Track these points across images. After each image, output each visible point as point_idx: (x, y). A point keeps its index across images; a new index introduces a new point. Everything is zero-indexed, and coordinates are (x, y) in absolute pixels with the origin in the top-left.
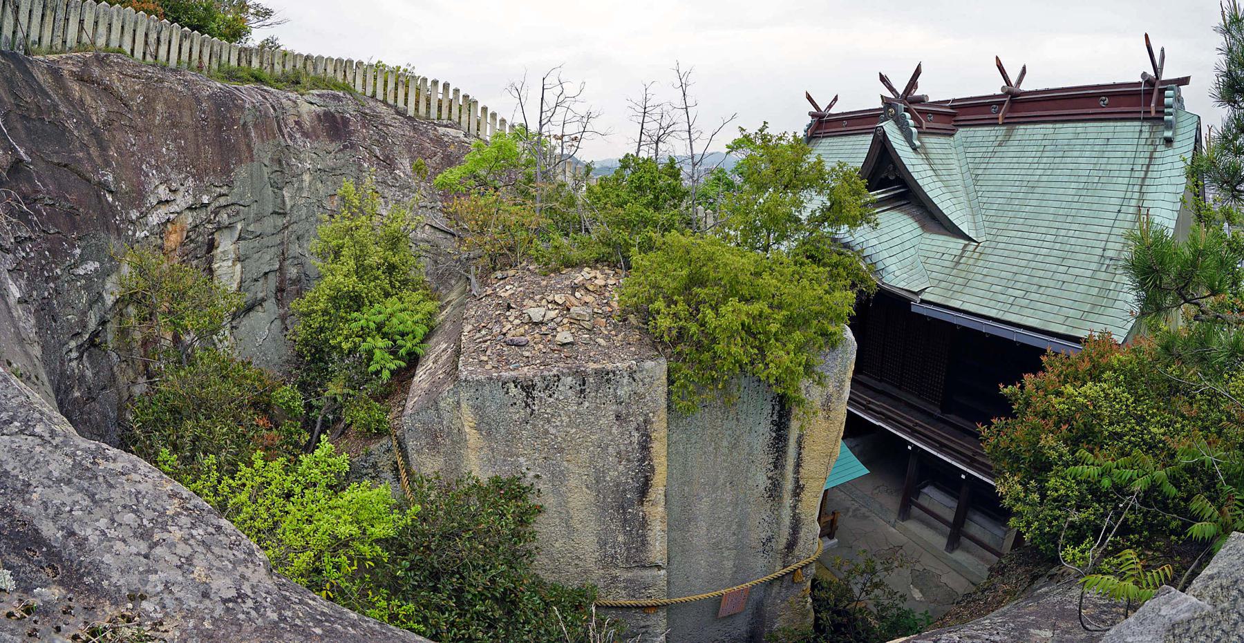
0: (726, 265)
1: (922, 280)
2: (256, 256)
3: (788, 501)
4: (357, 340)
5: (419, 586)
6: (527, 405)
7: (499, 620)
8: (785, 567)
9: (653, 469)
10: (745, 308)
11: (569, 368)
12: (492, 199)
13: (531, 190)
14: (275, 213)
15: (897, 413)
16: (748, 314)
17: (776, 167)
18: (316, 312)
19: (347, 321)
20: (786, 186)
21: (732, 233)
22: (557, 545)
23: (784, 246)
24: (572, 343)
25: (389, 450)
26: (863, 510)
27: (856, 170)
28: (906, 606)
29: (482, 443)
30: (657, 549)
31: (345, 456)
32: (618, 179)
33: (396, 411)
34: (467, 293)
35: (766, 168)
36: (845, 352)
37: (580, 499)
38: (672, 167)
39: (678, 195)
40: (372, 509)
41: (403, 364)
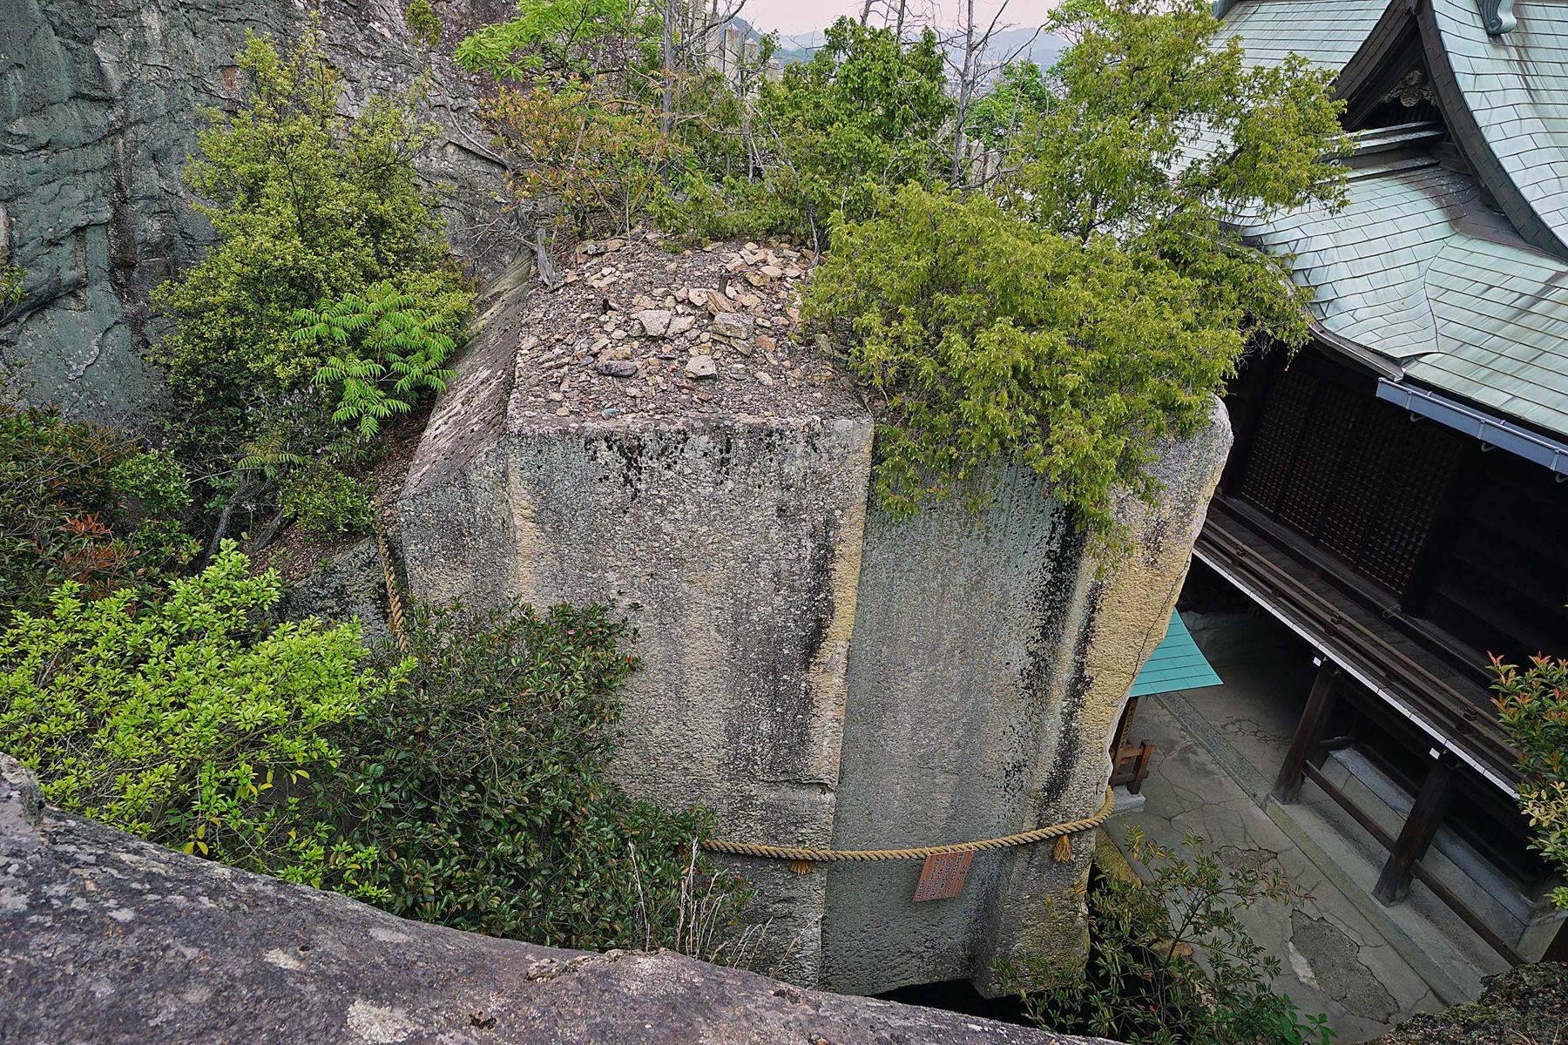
0: (999, 254)
1: (1418, 336)
2: (46, 191)
3: (1059, 701)
4: (308, 361)
5: (397, 812)
6: (628, 481)
7: (535, 872)
8: (1040, 826)
9: (831, 609)
10: (1024, 338)
11: (704, 420)
12: (575, 98)
13: (653, 83)
14: (77, 96)
15: (1301, 589)
16: (1027, 351)
17: (1135, 62)
18: (213, 308)
19: (286, 325)
20: (1149, 105)
21: (1028, 197)
22: (656, 731)
23: (1123, 229)
24: (713, 377)
25: (370, 563)
26: (1203, 757)
27: (1326, 76)
28: (1277, 987)
29: (543, 545)
30: (824, 755)
31: (272, 574)
32: (822, 70)
33: (387, 492)
34: (529, 278)
35: (1115, 65)
36: (1205, 447)
37: (703, 649)
38: (928, 52)
39: (931, 110)
40: (325, 665)
41: (404, 407)
